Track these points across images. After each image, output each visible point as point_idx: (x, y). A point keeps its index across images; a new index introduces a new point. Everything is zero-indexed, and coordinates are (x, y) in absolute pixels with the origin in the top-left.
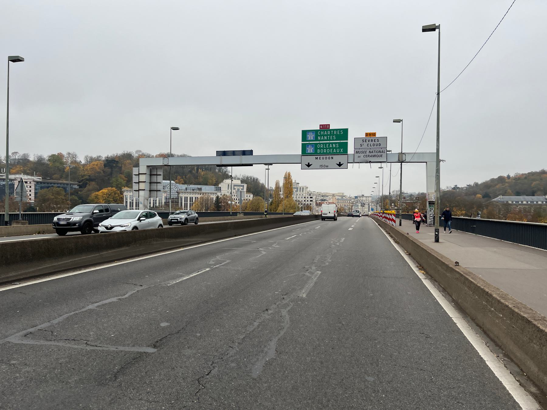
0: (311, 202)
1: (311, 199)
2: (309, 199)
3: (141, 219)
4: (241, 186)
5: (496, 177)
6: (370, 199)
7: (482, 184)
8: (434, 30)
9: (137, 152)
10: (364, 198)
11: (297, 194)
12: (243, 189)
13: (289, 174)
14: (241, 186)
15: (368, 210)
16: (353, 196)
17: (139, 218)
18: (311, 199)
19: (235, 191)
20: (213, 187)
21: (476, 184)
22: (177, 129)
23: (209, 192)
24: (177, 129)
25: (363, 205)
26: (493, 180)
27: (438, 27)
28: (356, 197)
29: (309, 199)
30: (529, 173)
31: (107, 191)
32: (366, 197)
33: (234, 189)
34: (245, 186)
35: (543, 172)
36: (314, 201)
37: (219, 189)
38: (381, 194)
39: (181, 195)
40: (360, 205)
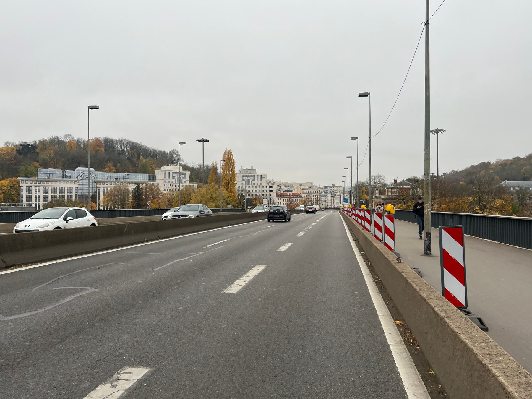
0: (271, 193)
1: (271, 189)
2: (269, 189)
3: (68, 218)
4: (183, 174)
5: (477, 163)
6: (342, 189)
7: (496, 165)
8: (367, 96)
9: (66, 136)
10: (335, 189)
11: (254, 184)
12: (185, 178)
13: (230, 153)
14: (183, 174)
15: (339, 201)
16: (322, 186)
17: (67, 216)
18: (271, 189)
19: (174, 180)
20: (146, 176)
21: (518, 159)
22: (184, 143)
23: (133, 180)
24: (184, 143)
25: (334, 196)
26: (473, 167)
27: (369, 94)
28: (326, 187)
29: (269, 189)
30: (514, 158)
31: (8, 181)
32: (337, 187)
33: (173, 177)
34: (188, 173)
35: (531, 157)
36: (275, 191)
37: (154, 179)
38: (354, 182)
39: (98, 186)
40: (330, 195)
